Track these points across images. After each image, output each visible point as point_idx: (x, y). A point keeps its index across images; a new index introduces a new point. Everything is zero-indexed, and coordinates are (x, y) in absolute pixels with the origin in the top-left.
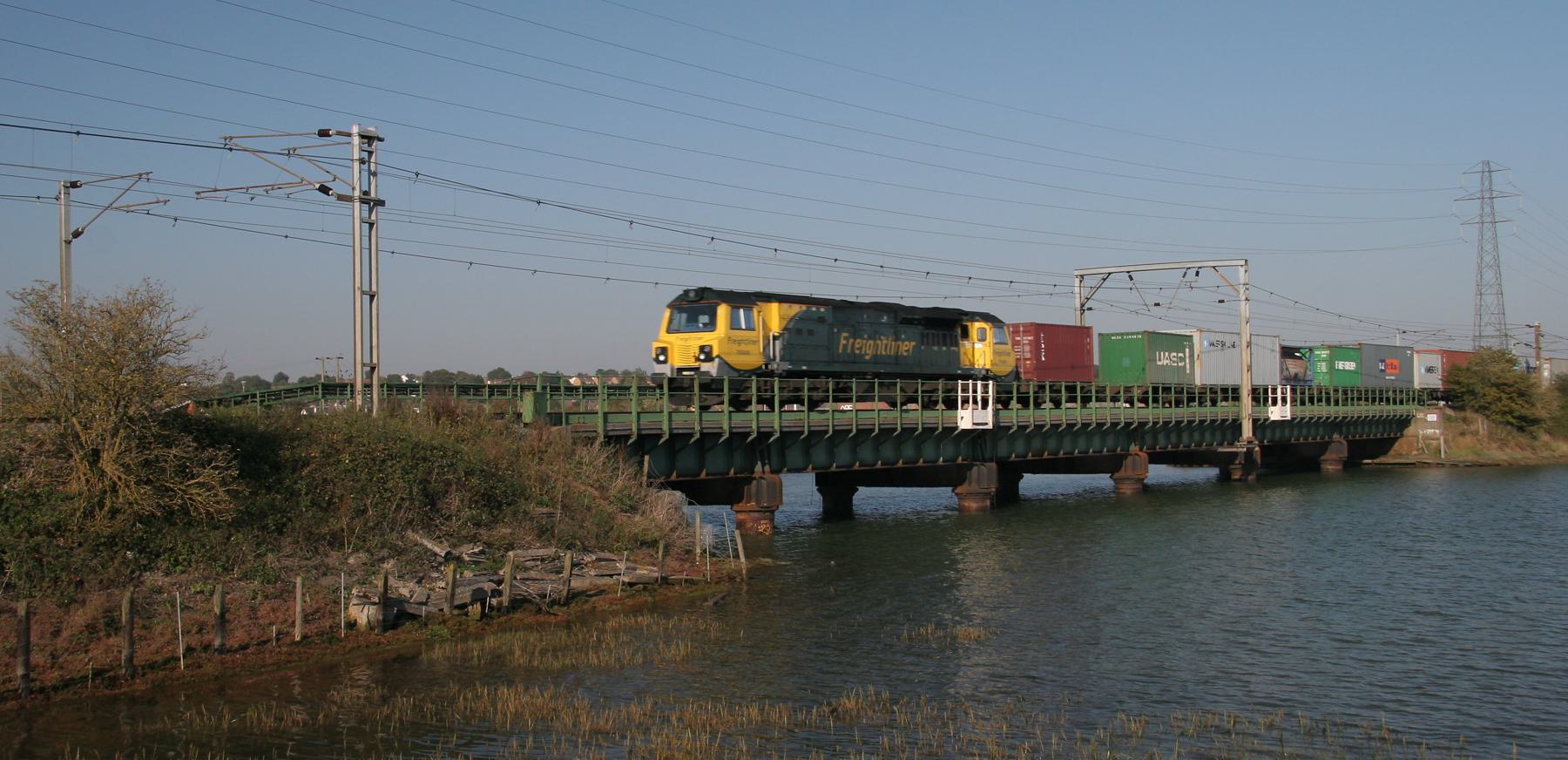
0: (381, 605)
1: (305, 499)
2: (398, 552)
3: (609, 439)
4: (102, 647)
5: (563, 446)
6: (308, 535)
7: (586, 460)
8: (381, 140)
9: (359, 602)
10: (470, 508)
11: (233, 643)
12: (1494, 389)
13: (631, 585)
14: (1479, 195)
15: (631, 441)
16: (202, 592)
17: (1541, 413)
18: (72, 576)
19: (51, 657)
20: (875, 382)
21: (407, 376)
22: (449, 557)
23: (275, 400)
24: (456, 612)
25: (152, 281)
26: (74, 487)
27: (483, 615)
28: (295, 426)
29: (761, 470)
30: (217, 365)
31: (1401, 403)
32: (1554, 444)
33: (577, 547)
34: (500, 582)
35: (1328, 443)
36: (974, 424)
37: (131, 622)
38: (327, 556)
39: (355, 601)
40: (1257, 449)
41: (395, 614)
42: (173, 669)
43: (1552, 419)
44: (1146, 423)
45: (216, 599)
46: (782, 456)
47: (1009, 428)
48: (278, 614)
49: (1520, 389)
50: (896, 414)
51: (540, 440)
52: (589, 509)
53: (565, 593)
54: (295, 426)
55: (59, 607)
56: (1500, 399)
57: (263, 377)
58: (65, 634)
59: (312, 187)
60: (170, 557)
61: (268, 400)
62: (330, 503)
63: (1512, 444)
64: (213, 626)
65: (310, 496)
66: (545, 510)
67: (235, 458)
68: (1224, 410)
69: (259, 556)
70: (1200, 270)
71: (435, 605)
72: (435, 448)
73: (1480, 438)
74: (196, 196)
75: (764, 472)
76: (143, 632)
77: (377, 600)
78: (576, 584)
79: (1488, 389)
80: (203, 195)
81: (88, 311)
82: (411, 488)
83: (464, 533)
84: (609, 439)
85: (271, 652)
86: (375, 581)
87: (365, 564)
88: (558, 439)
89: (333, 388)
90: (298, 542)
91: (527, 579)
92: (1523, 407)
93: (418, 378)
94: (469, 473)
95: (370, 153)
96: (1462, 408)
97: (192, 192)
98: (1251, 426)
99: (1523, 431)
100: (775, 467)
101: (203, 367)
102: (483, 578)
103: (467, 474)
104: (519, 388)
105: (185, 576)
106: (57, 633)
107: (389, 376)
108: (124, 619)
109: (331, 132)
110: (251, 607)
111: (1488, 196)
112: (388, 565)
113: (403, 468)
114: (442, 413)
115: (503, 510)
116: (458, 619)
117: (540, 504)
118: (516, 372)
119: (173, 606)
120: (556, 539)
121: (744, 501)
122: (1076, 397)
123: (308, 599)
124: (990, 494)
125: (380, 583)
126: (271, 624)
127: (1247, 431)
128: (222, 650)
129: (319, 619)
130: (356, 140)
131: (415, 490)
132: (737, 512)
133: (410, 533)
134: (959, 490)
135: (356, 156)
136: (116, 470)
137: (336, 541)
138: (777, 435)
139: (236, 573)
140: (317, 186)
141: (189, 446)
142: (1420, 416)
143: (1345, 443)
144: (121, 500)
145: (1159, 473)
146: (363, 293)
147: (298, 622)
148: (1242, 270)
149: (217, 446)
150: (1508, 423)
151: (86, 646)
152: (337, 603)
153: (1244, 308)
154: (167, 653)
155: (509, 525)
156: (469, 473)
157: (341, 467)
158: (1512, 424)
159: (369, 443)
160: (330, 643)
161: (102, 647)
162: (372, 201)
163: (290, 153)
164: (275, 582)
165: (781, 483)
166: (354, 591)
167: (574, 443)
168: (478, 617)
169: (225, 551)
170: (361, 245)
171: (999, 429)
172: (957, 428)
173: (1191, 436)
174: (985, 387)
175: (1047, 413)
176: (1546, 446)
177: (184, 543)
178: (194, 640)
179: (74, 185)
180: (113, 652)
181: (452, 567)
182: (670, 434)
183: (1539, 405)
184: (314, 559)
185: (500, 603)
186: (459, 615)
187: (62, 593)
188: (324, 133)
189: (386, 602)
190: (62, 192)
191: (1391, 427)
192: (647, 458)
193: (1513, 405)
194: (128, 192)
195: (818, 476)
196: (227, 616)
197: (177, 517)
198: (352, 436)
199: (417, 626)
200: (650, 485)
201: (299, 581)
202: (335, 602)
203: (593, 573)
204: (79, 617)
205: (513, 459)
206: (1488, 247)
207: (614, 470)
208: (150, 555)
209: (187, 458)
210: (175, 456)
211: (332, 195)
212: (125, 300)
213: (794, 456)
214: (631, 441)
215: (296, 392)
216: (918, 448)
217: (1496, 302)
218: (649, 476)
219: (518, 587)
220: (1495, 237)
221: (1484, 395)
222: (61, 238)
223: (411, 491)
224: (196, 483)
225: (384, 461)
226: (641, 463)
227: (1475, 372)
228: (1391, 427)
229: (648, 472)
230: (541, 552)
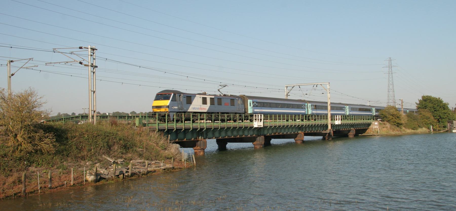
0: (95, 176)
1: (75, 147)
2: (100, 161)
3: (159, 130)
4: (17, 188)
5: (146, 132)
6: (75, 157)
7: (153, 136)
8: (96, 50)
9: (89, 175)
10: (120, 149)
11: (53, 186)
12: (391, 116)
13: (164, 169)
14: (388, 66)
15: (165, 131)
16: (45, 172)
17: (402, 122)
18: (9, 169)
19: (2, 190)
20: (268, 115)
21: (108, 113)
22: (114, 162)
23: (68, 120)
24: (116, 177)
25: (32, 88)
26: (10, 144)
27: (123, 178)
28: (72, 127)
29: (201, 138)
30: (50, 111)
31: (369, 120)
32: (406, 130)
33: (150, 160)
34: (128, 169)
35: (350, 130)
36: (258, 126)
37: (25, 181)
38: (80, 162)
39: (88, 174)
40: (332, 132)
41: (99, 178)
42: (37, 193)
43: (405, 123)
44: (303, 125)
45: (49, 174)
46: (207, 134)
47: (267, 127)
48: (67, 178)
49: (397, 116)
50: (212, 124)
51: (140, 131)
52: (153, 149)
53: (146, 172)
54: (72, 127)
55: (5, 177)
56: (393, 119)
57: (68, 114)
58: (7, 184)
59: (77, 62)
60: (37, 163)
61: (66, 120)
62: (82, 148)
63: (396, 130)
64: (48, 182)
65: (76, 146)
66: (141, 149)
67: (55, 136)
68: (323, 122)
69: (61, 162)
70: (317, 85)
71: (110, 175)
72: (111, 133)
73: (388, 128)
74: (45, 64)
75: (202, 139)
76: (29, 183)
77: (94, 174)
78: (149, 169)
79: (390, 116)
80: (47, 64)
81: (13, 96)
82: (104, 144)
83: (118, 156)
84: (159, 130)
85: (64, 188)
86: (94, 169)
87: (91, 164)
88: (145, 130)
89: (85, 117)
90: (72, 159)
91: (136, 168)
92: (398, 120)
93: (111, 114)
94: (120, 140)
95: (94, 53)
96: (384, 121)
97: (44, 64)
98: (330, 126)
99: (398, 127)
100: (205, 138)
101: (46, 111)
102: (124, 168)
103: (119, 140)
104: (136, 116)
105: (41, 168)
106: (4, 184)
107: (103, 113)
108: (23, 180)
109: (83, 48)
110: (59, 176)
111: (390, 67)
112: (97, 165)
113: (102, 138)
114: (114, 123)
115: (129, 150)
116: (117, 179)
117: (139, 148)
118: (138, 112)
119: (37, 176)
120: (144, 157)
121: (196, 146)
122: (281, 119)
123: (75, 174)
124: (262, 144)
125: (95, 169)
126: (64, 181)
127: (329, 127)
128: (51, 188)
129: (78, 179)
130: (90, 50)
131: (105, 144)
132: (195, 150)
133: (103, 156)
134: (254, 143)
135: (90, 54)
136: (22, 139)
137: (83, 158)
138: (205, 129)
139: (55, 167)
140: (79, 62)
141: (42, 133)
142: (373, 123)
143: (354, 130)
144: (23, 148)
145: (307, 138)
146: (92, 91)
147: (72, 180)
148: (328, 85)
149: (50, 133)
150: (395, 125)
151: (13, 187)
152: (83, 175)
153: (329, 95)
154: (35, 189)
155: (131, 153)
156: (120, 140)
157: (85, 138)
158: (396, 125)
159: (92, 132)
160: (81, 186)
161: (17, 188)
162: (94, 66)
163: (71, 53)
164: (66, 170)
165: (206, 142)
166: (88, 172)
167: (150, 132)
168: (122, 178)
169: (52, 161)
170: (91, 78)
171: (265, 127)
172: (253, 127)
173: (315, 128)
174: (261, 116)
175: (277, 123)
176: (404, 130)
177: (41, 159)
178: (43, 185)
179: (12, 61)
180: (20, 189)
181: (115, 165)
182: (176, 129)
183: (402, 120)
184: (77, 163)
185: (128, 175)
186: (117, 178)
187: (6, 173)
188: (81, 48)
189: (97, 174)
190: (8, 63)
191: (366, 126)
192: (169, 135)
193: (396, 120)
194: (26, 62)
195: (217, 140)
196: (52, 179)
197: (37, 151)
198: (88, 130)
199: (105, 181)
200: (170, 143)
201: (72, 169)
202: (83, 175)
203: (154, 166)
204: (11, 179)
205: (133, 136)
206: (391, 79)
207: (160, 138)
208: (31, 163)
209: (42, 136)
210: (38, 136)
211: (83, 64)
212: (24, 93)
213: (210, 134)
214: (165, 131)
215: (70, 118)
216: (243, 132)
217: (393, 93)
218: (170, 140)
219: (133, 170)
220: (392, 77)
221: (389, 117)
222: (8, 76)
223: (104, 145)
224: (44, 143)
225: (96, 137)
226: (168, 137)
227: (387, 112)
228: (366, 126)
229: (170, 139)
230: (140, 161)
